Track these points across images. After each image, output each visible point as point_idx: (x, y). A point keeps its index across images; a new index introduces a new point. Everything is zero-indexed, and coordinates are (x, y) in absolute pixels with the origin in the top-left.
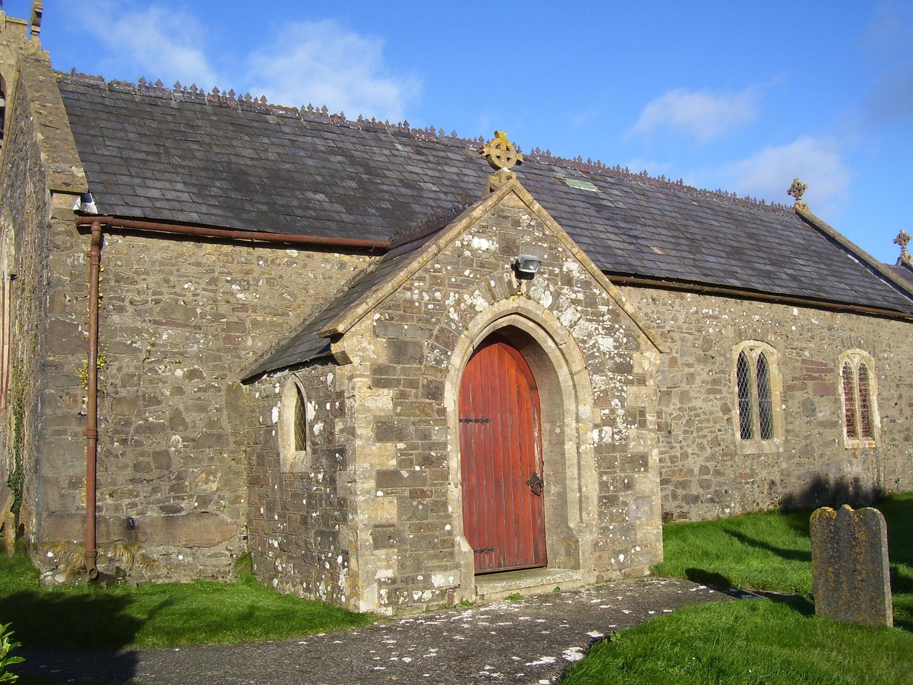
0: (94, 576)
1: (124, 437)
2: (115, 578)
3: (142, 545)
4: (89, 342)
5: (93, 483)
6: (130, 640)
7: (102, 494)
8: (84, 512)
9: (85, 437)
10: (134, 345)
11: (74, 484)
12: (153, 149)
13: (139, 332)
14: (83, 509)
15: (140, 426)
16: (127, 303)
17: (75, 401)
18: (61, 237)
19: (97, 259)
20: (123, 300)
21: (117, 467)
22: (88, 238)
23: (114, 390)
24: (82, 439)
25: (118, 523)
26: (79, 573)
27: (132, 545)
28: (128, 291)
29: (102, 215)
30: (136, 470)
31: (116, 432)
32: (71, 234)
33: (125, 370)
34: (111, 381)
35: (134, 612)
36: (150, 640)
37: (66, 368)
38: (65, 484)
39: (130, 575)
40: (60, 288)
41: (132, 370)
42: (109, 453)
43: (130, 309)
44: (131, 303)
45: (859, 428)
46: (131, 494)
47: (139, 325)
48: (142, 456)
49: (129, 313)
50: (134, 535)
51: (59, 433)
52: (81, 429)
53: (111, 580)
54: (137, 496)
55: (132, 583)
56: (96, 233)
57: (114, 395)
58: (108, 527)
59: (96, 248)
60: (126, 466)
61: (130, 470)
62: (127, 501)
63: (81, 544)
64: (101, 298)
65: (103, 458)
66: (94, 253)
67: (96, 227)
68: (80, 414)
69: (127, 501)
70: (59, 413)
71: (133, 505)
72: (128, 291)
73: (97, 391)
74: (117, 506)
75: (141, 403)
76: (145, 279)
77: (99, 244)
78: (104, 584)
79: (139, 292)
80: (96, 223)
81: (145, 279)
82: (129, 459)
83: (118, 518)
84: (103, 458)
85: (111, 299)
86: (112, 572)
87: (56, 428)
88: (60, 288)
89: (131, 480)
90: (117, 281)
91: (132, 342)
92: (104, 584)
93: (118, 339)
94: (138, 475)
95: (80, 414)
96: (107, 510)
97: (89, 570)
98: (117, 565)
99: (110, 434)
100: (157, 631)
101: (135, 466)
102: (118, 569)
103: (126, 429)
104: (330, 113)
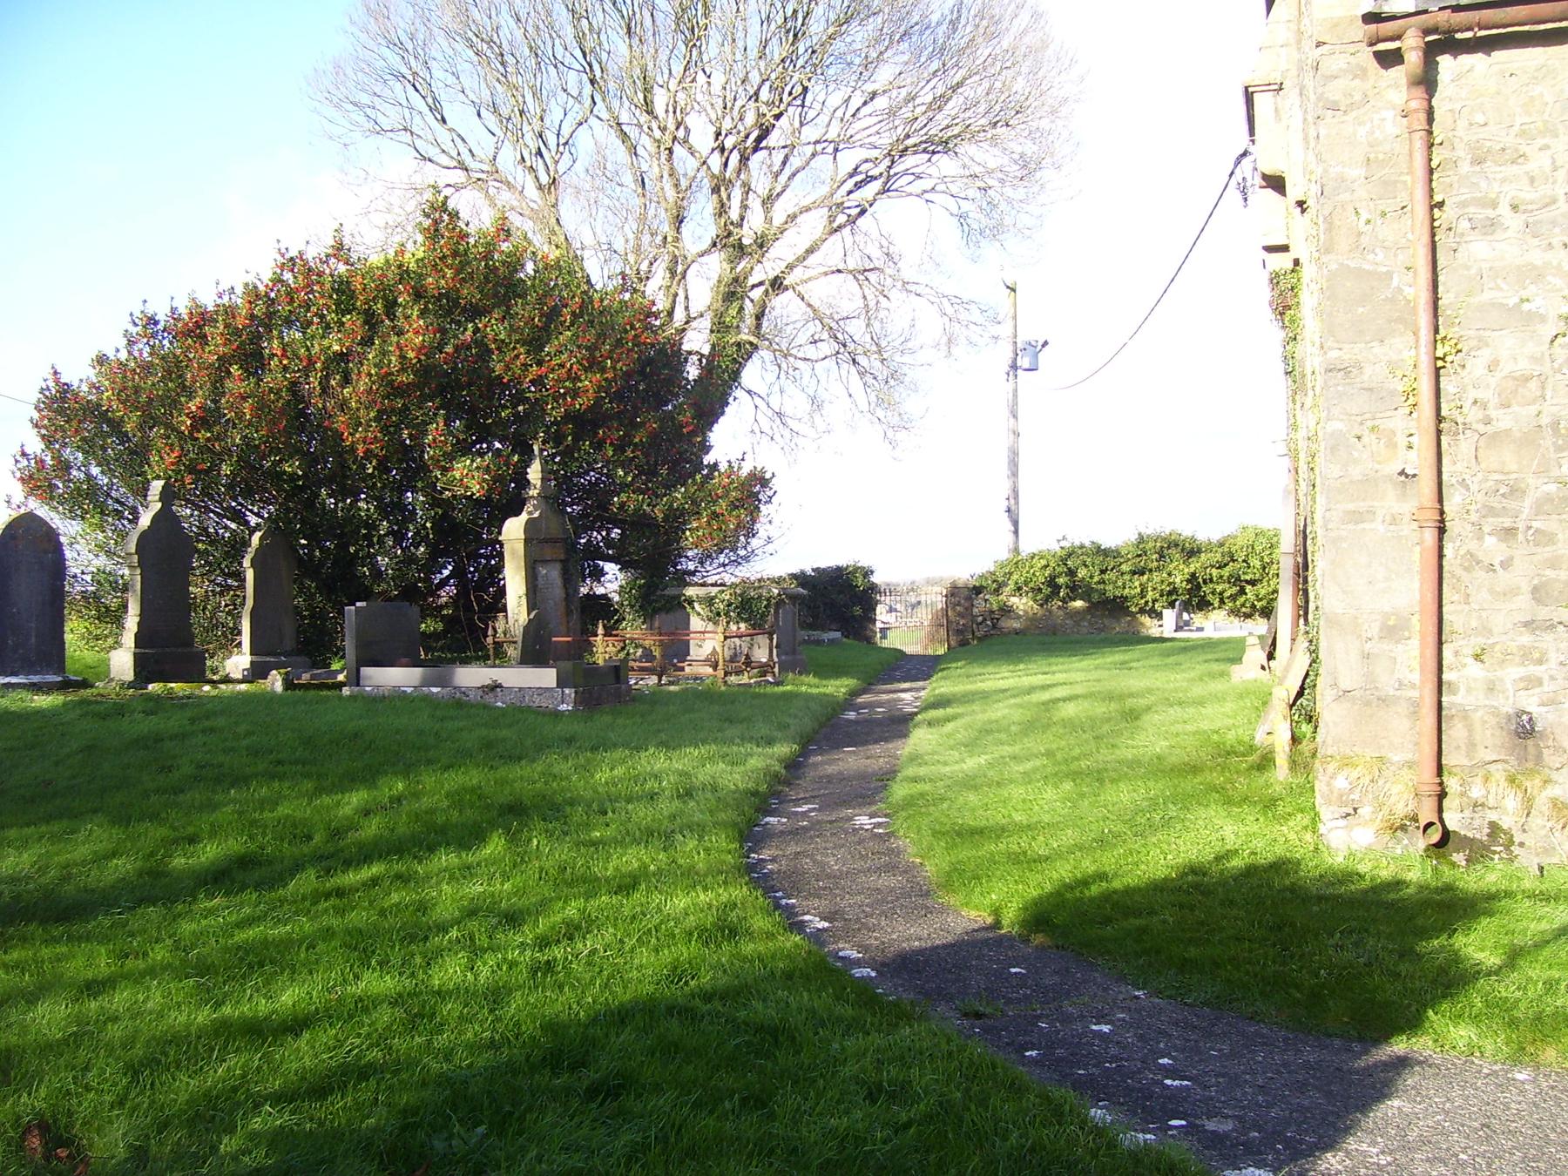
0: (1435, 836)
1: (1508, 523)
2: (1487, 848)
3: (1555, 776)
4: (1414, 311)
5: (1433, 629)
6: (1412, 1024)
7: (1456, 653)
8: (1415, 694)
9: (1415, 525)
10: (1526, 306)
11: (1393, 631)
13: (1537, 274)
14: (1413, 686)
15: (1548, 499)
16: (1504, 210)
17: (1391, 445)
18: (1341, 83)
19: (1423, 116)
20: (1494, 205)
21: (1492, 591)
22: (1398, 74)
23: (1480, 415)
24: (1408, 529)
25: (1493, 721)
26: (1403, 828)
27: (1530, 773)
28: (1504, 180)
29: (1425, 12)
30: (1538, 601)
31: (1491, 511)
32: (1362, 73)
33: (1506, 367)
34: (1472, 394)
35: (1477, 945)
36: (1462, 1034)
37: (1368, 371)
38: (1374, 630)
39: (1522, 845)
40: (1346, 197)
41: (1523, 365)
42: (1472, 561)
43: (1514, 222)
44: (1515, 208)
46: (1526, 656)
47: (1537, 257)
48: (1553, 567)
49: (1509, 233)
50: (1531, 750)
51: (1356, 517)
52: (1407, 507)
53: (1478, 852)
54: (1540, 662)
55: (1528, 861)
56: (1413, 58)
57: (1482, 428)
58: (1470, 730)
59: (1420, 92)
60: (1513, 592)
61: (1523, 601)
62: (1514, 672)
63: (1410, 765)
64: (1441, 205)
65: (1459, 572)
66: (1414, 104)
67: (1412, 46)
68: (1402, 473)
69: (1514, 672)
70: (1356, 472)
71: (1532, 683)
72: (1504, 180)
73: (1439, 418)
74: (1492, 682)
75: (1548, 441)
76: (1547, 147)
77: (1427, 81)
78: (1459, 858)
79: (1532, 180)
80: (1411, 33)
81: (1547, 147)
82: (1521, 575)
83: (1495, 712)
84: (1459, 572)
85: (1464, 204)
86: (1482, 835)
87: (1351, 506)
88: (1346, 197)
89: (1526, 624)
90: (1478, 161)
91: (1522, 301)
92: (1459, 858)
93: (1487, 296)
94: (1543, 613)
95: (1402, 473)
96: (1469, 690)
97: (1422, 824)
98: (1492, 816)
99: (1474, 517)
100: (1503, 1014)
101: (1535, 590)
102: (1494, 827)
103: (1512, 504)
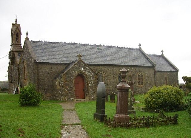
12: (42, 52)
45: (141, 83)
104: (64, 42)
